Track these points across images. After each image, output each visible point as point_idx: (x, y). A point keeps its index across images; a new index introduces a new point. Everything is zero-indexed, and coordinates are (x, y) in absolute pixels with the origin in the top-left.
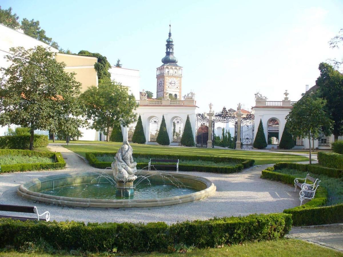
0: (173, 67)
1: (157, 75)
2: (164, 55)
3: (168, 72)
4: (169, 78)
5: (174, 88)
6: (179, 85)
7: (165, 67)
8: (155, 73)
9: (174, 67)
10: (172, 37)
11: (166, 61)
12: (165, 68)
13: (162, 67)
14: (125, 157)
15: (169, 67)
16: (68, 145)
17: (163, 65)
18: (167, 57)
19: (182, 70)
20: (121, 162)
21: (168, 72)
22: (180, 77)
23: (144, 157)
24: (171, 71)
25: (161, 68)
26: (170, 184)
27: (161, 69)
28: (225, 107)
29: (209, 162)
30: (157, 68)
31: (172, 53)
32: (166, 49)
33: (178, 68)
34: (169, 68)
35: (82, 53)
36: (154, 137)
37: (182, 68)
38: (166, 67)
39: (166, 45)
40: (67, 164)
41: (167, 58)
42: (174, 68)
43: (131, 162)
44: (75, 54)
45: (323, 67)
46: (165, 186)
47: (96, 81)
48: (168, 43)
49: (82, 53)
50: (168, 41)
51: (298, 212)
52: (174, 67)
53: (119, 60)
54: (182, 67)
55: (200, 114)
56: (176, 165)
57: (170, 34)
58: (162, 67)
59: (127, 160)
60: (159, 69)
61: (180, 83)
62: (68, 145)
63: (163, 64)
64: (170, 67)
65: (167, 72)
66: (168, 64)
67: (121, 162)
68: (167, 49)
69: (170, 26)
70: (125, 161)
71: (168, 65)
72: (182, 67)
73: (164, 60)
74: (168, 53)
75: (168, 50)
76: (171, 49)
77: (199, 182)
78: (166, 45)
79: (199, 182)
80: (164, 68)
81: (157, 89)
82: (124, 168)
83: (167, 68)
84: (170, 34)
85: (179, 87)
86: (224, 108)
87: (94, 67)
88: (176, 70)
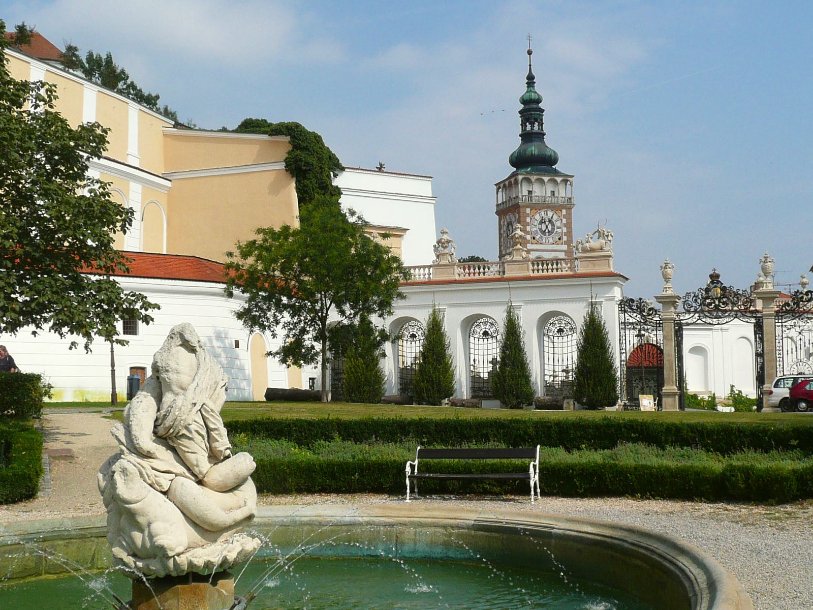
0: (543, 178)
1: (498, 205)
2: (516, 143)
3: (530, 192)
5: (551, 241)
6: (565, 230)
7: (520, 177)
8: (492, 199)
9: (549, 178)
10: (537, 87)
11: (519, 161)
12: (520, 180)
13: (513, 180)
14: (168, 423)
15: (533, 178)
17: (514, 175)
18: (525, 146)
19: (571, 184)
20: (148, 456)
21: (530, 192)
22: (568, 206)
23: (406, 434)
24: (537, 190)
25: (510, 182)
27: (507, 185)
30: (496, 185)
31: (541, 135)
33: (559, 179)
34: (533, 180)
35: (249, 126)
36: (486, 385)
37: (570, 179)
38: (523, 179)
39: (520, 112)
41: (525, 151)
42: (546, 179)
43: (215, 457)
44: (233, 131)
46: (425, 588)
47: (290, 205)
48: (527, 107)
49: (249, 126)
50: (527, 97)
52: (549, 178)
53: (381, 165)
54: (572, 176)
55: (633, 301)
56: (526, 470)
57: (531, 79)
58: (513, 180)
59: (185, 442)
60: (502, 185)
61: (569, 225)
64: (535, 177)
65: (525, 193)
66: (529, 169)
67: (148, 456)
68: (523, 125)
69: (530, 53)
70: (173, 450)
71: (528, 173)
72: (572, 176)
73: (517, 158)
74: (527, 137)
76: (537, 123)
77: (638, 562)
78: (520, 112)
79: (638, 562)
80: (516, 182)
81: (500, 246)
82: (165, 493)
83: (528, 181)
84: (531, 79)
85: (565, 238)
86: (711, 276)
87: (282, 166)
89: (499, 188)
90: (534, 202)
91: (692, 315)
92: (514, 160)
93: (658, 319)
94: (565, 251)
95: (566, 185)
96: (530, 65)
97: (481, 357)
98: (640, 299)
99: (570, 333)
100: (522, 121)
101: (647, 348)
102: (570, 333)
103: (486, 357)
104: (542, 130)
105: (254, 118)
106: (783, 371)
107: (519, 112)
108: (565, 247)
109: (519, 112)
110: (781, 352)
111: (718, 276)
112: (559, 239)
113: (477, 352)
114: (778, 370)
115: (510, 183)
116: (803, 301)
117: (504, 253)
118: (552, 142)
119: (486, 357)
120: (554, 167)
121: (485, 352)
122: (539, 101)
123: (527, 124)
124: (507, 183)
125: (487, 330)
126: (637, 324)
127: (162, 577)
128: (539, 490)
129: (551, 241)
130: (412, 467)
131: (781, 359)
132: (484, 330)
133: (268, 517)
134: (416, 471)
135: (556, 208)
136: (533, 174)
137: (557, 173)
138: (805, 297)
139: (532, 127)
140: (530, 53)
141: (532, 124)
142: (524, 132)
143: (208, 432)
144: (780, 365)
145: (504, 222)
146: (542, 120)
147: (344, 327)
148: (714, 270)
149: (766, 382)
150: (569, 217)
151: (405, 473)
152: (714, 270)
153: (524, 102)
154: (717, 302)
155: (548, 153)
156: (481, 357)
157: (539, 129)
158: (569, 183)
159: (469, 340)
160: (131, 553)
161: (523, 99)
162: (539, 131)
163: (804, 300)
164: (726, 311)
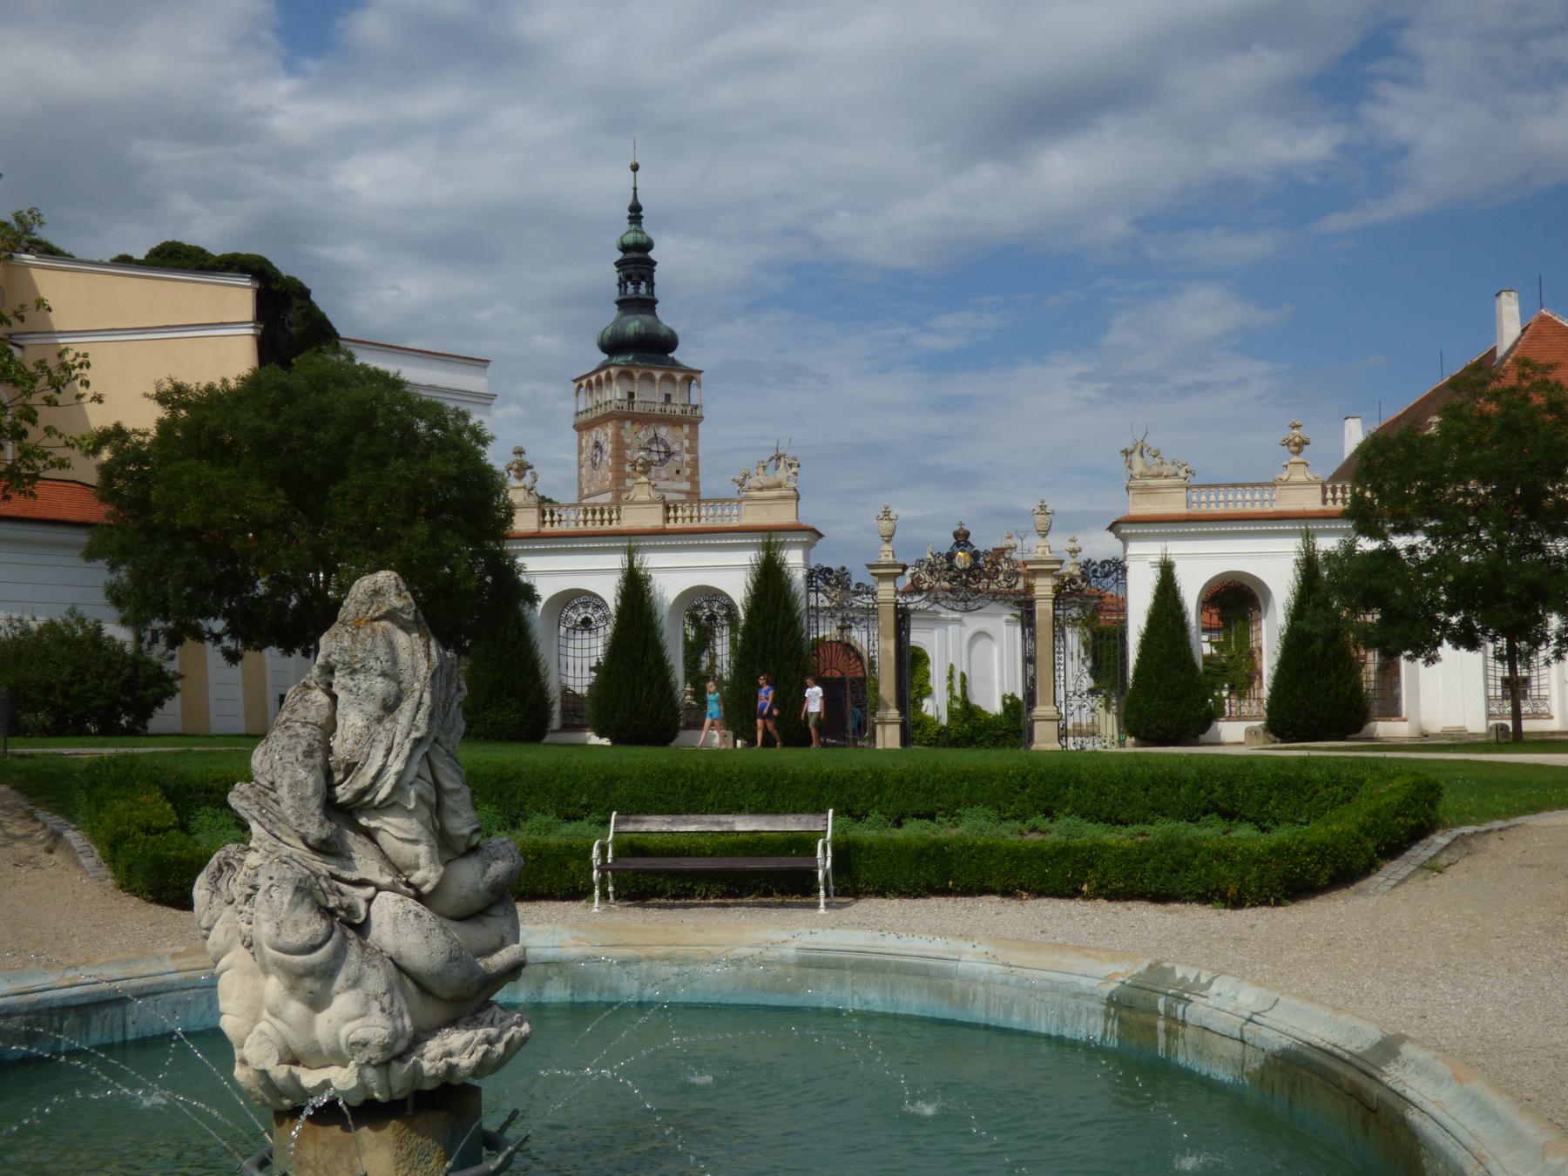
2: (607, 317)
4: (636, 427)
13: (603, 374)
16: (266, 1131)
17: (604, 366)
22: (690, 420)
26: (1076, 1018)
28: (966, 528)
29: (408, 594)
32: (619, 285)
33: (679, 376)
40: (104, 625)
42: (658, 375)
45: (493, 438)
48: (629, 255)
51: (358, 578)
55: (829, 571)
57: (636, 213)
58: (603, 374)
60: (584, 382)
62: (266, 1131)
63: (605, 357)
64: (641, 371)
68: (622, 284)
69: (635, 168)
73: (611, 337)
75: (626, 287)
76: (644, 284)
84: (636, 213)
86: (956, 535)
88: (668, 388)
89: (580, 386)
90: (636, 410)
91: (924, 596)
92: (606, 341)
93: (871, 601)
94: (687, 493)
95: (690, 384)
96: (635, 189)
97: (578, 661)
98: (843, 569)
99: (601, 625)
100: (620, 279)
101: (834, 650)
102: (601, 625)
103: (586, 661)
104: (652, 294)
105: (155, 246)
106: (1065, 686)
107: (615, 263)
108: (686, 486)
109: (615, 263)
110: (1062, 655)
111: (967, 534)
112: (678, 472)
113: (578, 653)
114: (1057, 684)
115: (599, 381)
116: (1096, 577)
117: (586, 492)
118: (668, 316)
119: (586, 661)
120: (670, 355)
121: (586, 653)
122: (648, 246)
123: (629, 283)
124: (593, 378)
125: (589, 616)
126: (836, 609)
127: (356, 1105)
128: (832, 887)
129: (664, 474)
130: (603, 849)
131: (1062, 667)
132: (583, 616)
133: (1295, 1038)
134: (610, 855)
135: (674, 422)
136: (635, 365)
137: (675, 365)
138: (1099, 569)
139: (637, 289)
140: (635, 168)
141: (637, 284)
142: (624, 297)
143: (439, 799)
144: (1060, 676)
145: (587, 442)
146: (652, 278)
147: (202, 618)
148: (961, 524)
149: (1038, 701)
150: (693, 437)
151: (592, 862)
152: (961, 524)
153: (625, 248)
154: (964, 577)
155: (664, 332)
156: (578, 661)
157: (648, 293)
158: (694, 382)
159: (559, 632)
160: (288, 1058)
161: (622, 243)
162: (647, 297)
163: (1098, 574)
164: (978, 591)
